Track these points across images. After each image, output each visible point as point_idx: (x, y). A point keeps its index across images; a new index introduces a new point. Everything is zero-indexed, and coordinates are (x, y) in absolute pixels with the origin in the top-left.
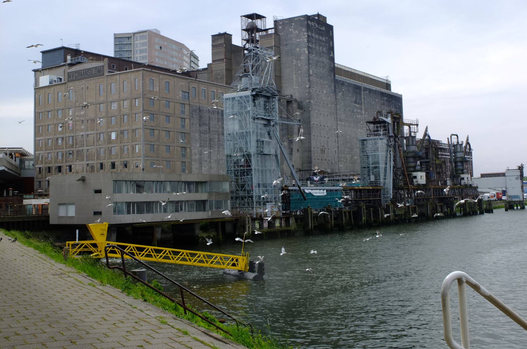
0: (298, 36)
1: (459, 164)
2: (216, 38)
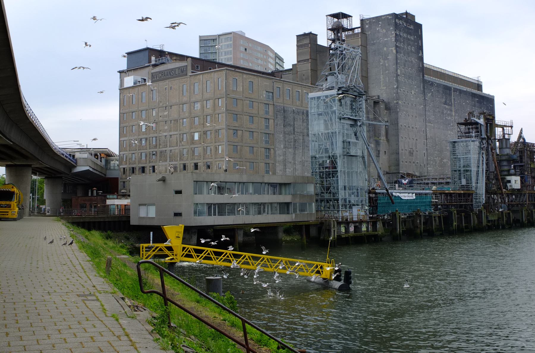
0: (385, 35)
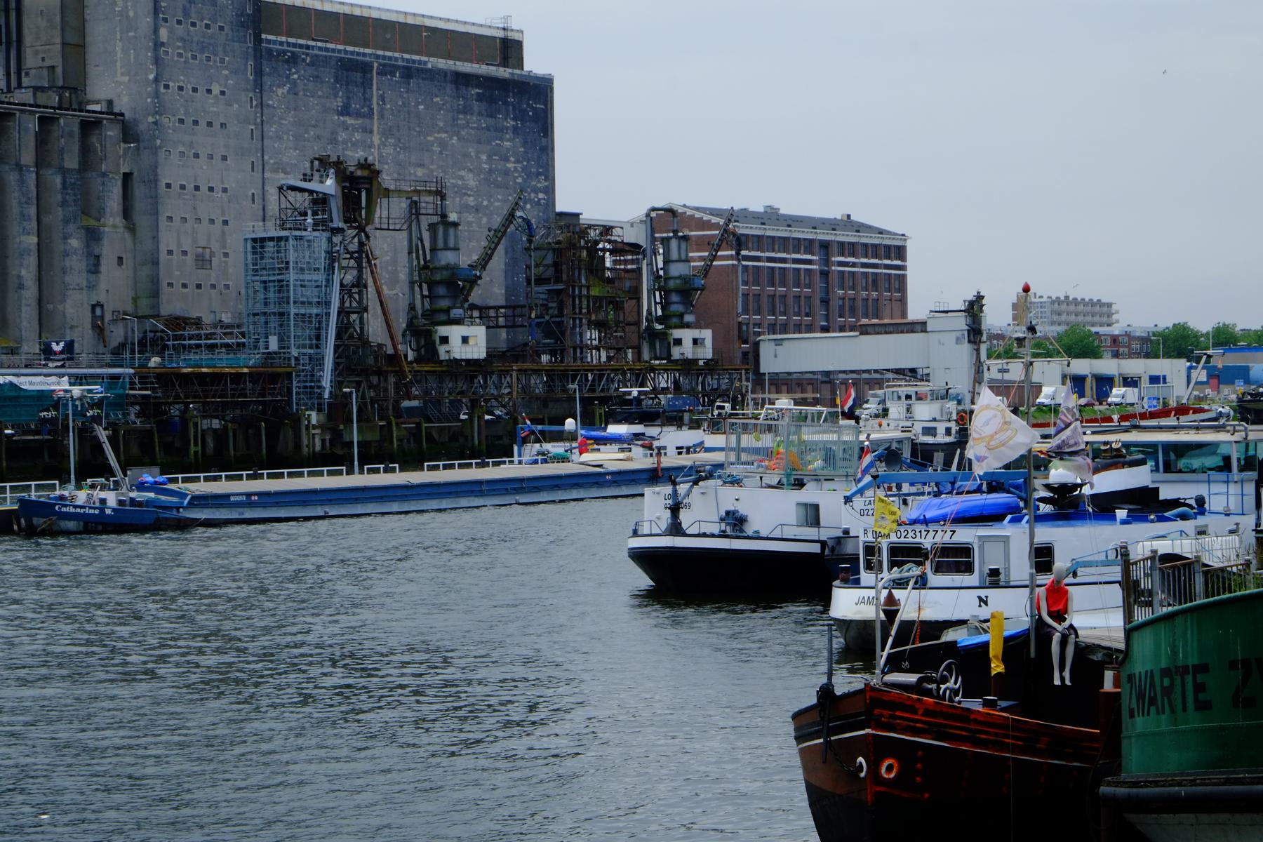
1: (675, 297)
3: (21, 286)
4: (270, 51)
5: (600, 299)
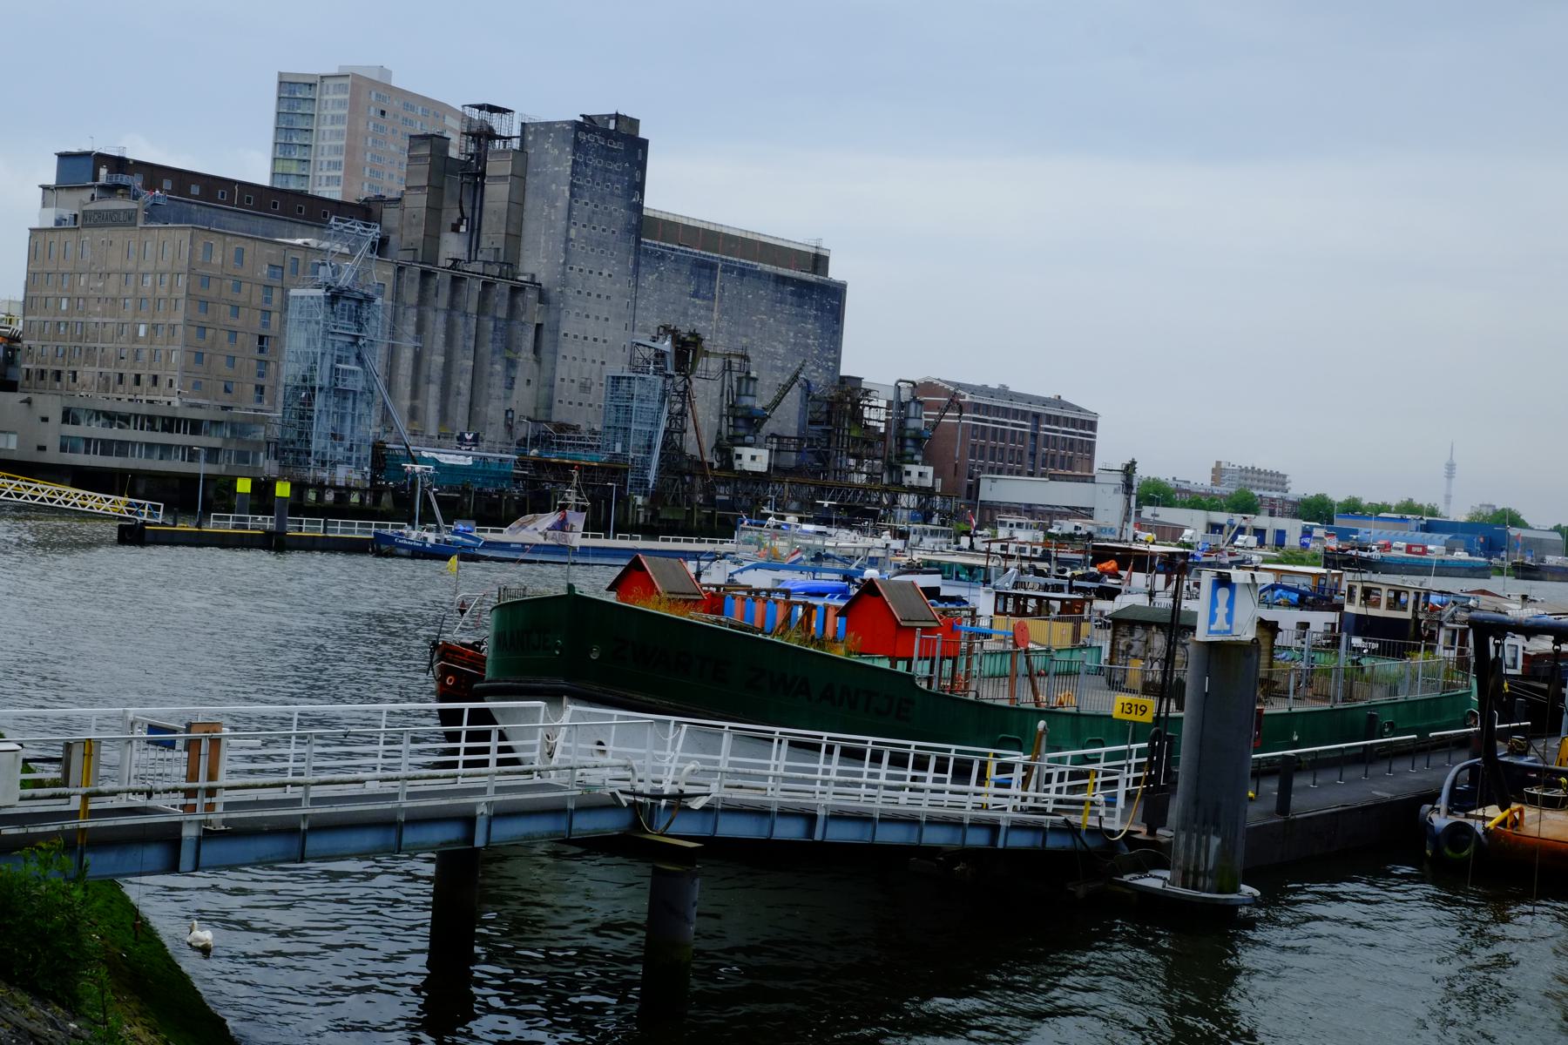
0: (557, 161)
1: (909, 443)
2: (417, 141)
3: (459, 394)
4: (646, 250)
5: (857, 439)
